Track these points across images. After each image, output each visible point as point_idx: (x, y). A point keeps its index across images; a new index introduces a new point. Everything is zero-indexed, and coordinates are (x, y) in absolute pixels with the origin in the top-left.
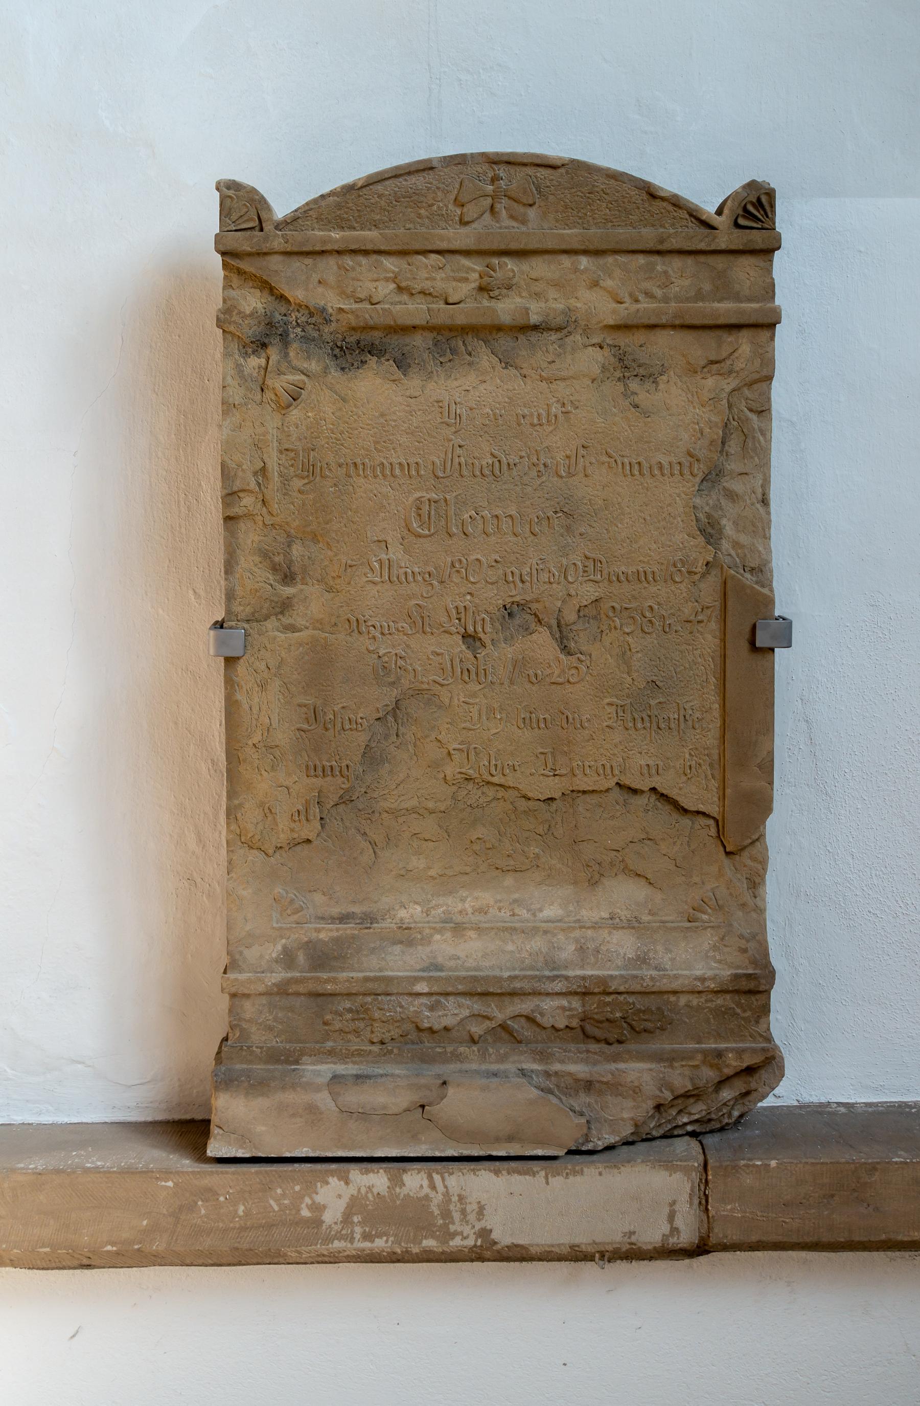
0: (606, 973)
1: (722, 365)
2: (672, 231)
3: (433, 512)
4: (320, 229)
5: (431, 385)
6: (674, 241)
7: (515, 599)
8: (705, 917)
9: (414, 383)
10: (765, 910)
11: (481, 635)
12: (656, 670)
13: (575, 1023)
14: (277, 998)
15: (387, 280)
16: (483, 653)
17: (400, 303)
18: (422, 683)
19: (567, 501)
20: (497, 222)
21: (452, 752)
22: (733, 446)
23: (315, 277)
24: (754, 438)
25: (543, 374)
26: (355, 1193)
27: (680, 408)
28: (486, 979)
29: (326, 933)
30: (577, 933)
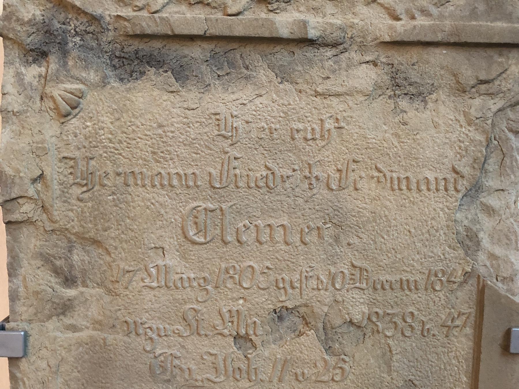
3: (208, 222)
5: (207, 97)
7: (284, 304)
9: (191, 95)
11: (253, 337)
12: (413, 370)
17: (178, 12)
19: (336, 213)
22: (492, 165)
24: (512, 156)
25: (318, 89)
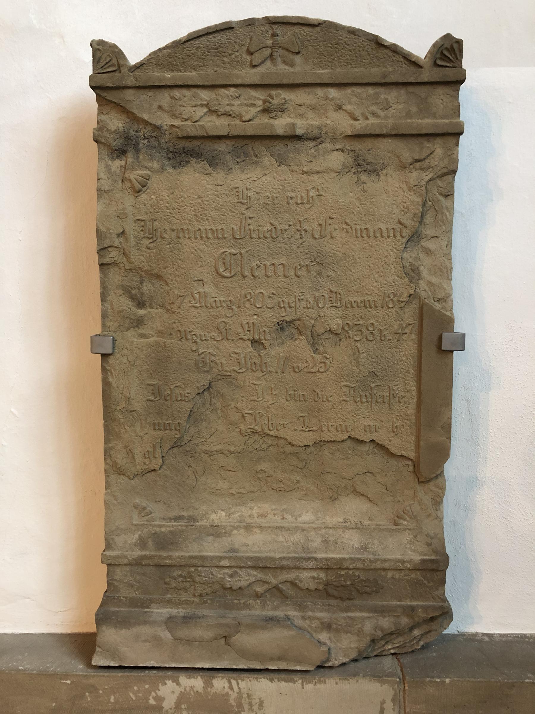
0: (341, 556)
1: (423, 163)
2: (391, 69)
4: (158, 72)
6: (392, 76)
7: (284, 318)
8: (405, 523)
9: (220, 176)
10: (443, 518)
11: (264, 341)
13: (321, 587)
14: (136, 567)
15: (202, 106)
16: (265, 353)
18: (226, 371)
20: (275, 66)
21: (245, 415)
22: (428, 219)
23: (155, 105)
24: (442, 213)
25: (304, 169)
26: (183, 691)
27: (393, 193)
28: (266, 558)
29: (167, 527)
30: (323, 531)
